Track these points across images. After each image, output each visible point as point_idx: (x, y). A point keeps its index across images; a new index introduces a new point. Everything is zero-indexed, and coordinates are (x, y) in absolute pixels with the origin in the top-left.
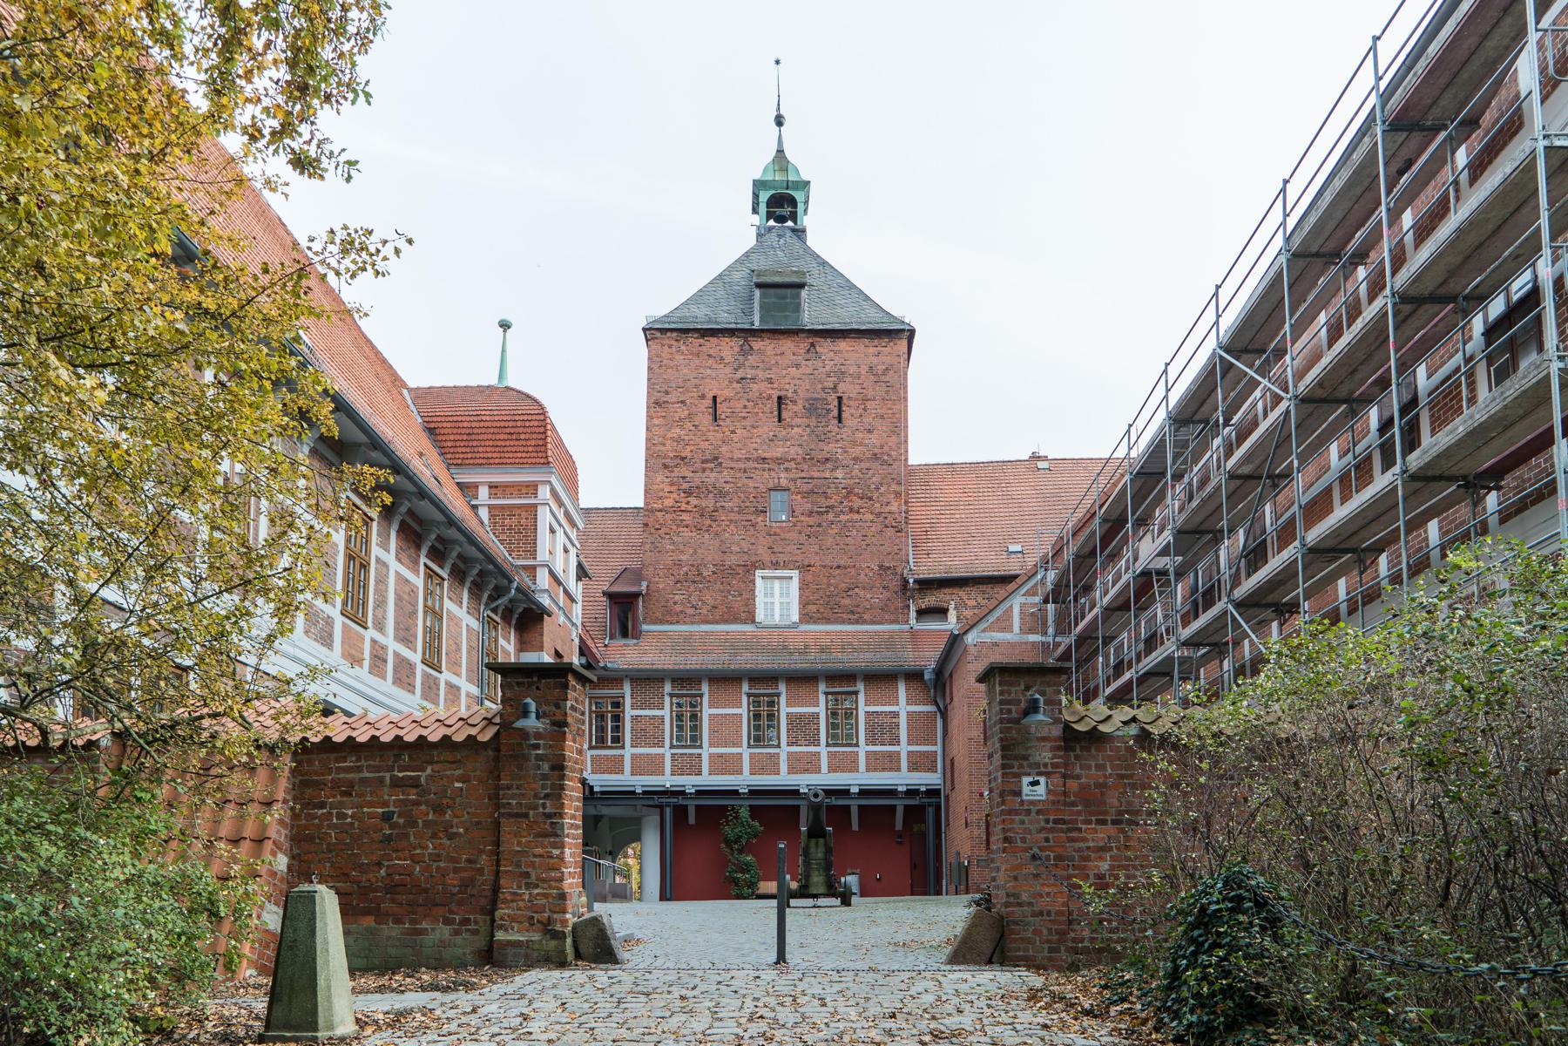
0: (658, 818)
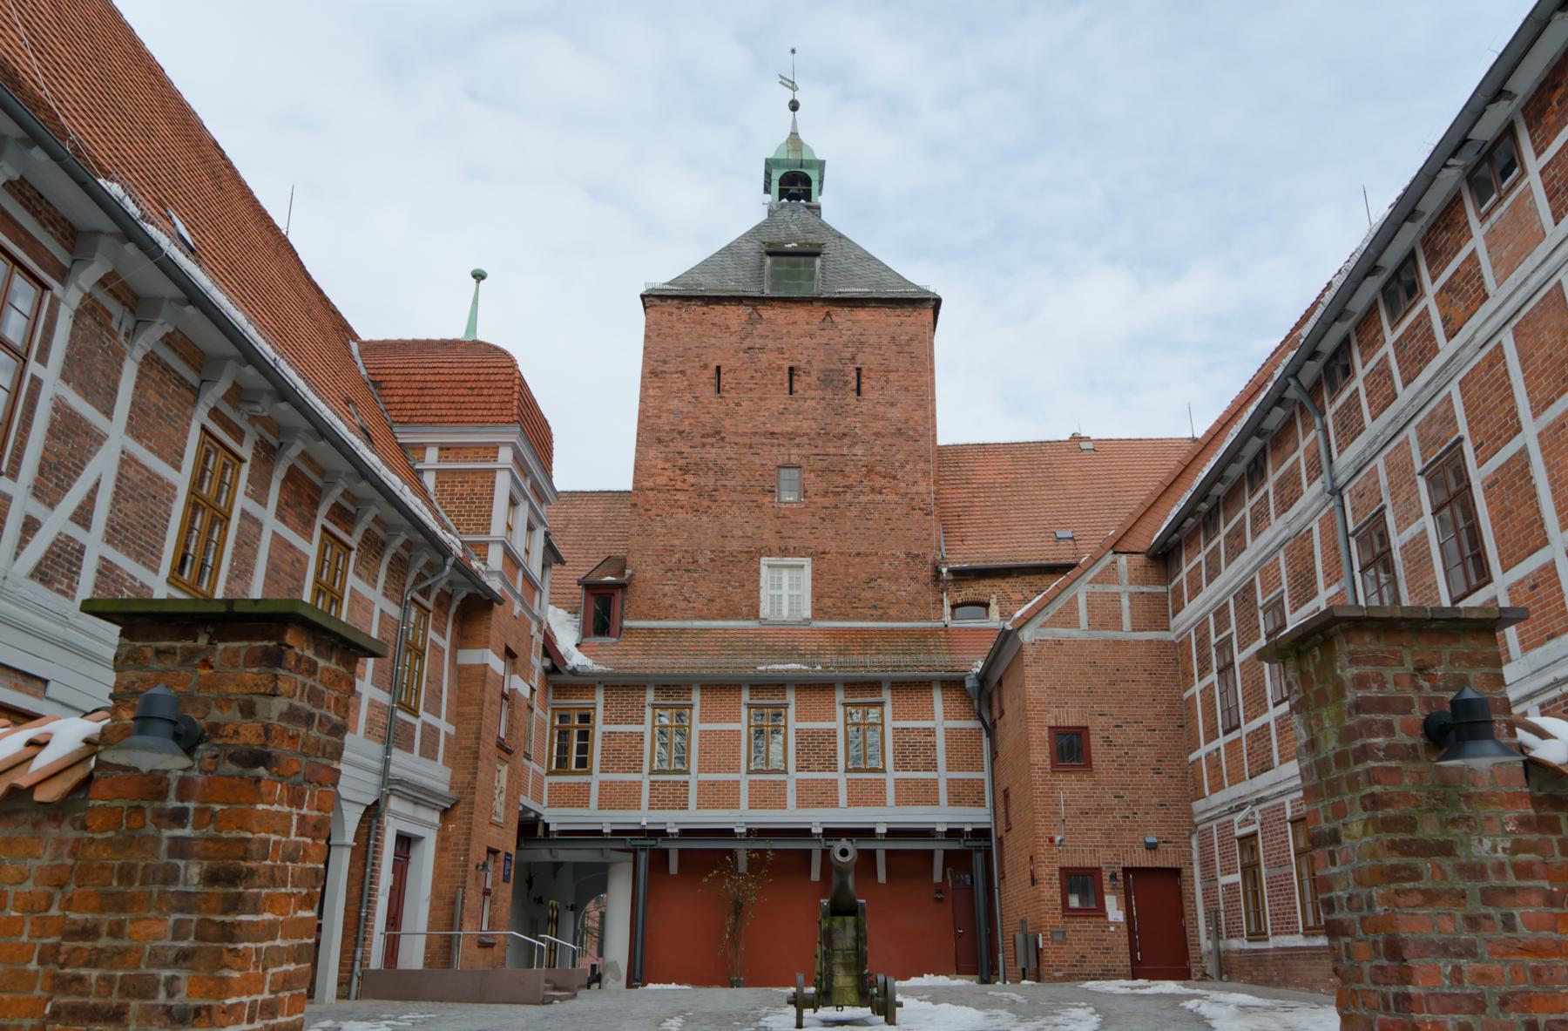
0: (631, 865)
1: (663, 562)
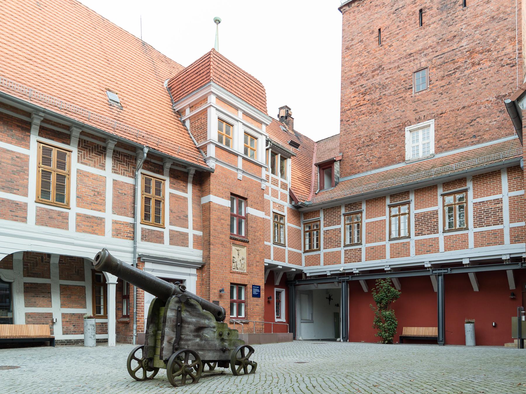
1: (356, 145)
